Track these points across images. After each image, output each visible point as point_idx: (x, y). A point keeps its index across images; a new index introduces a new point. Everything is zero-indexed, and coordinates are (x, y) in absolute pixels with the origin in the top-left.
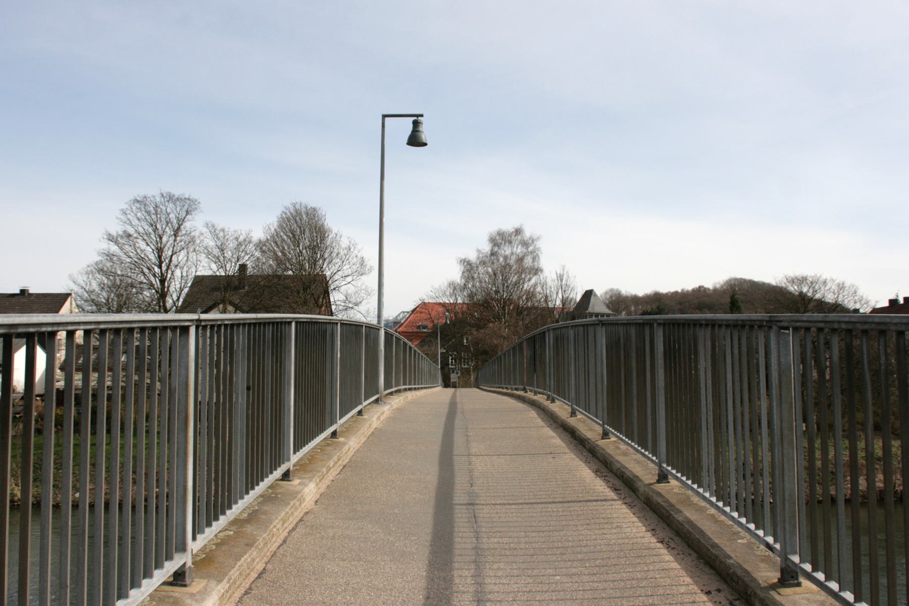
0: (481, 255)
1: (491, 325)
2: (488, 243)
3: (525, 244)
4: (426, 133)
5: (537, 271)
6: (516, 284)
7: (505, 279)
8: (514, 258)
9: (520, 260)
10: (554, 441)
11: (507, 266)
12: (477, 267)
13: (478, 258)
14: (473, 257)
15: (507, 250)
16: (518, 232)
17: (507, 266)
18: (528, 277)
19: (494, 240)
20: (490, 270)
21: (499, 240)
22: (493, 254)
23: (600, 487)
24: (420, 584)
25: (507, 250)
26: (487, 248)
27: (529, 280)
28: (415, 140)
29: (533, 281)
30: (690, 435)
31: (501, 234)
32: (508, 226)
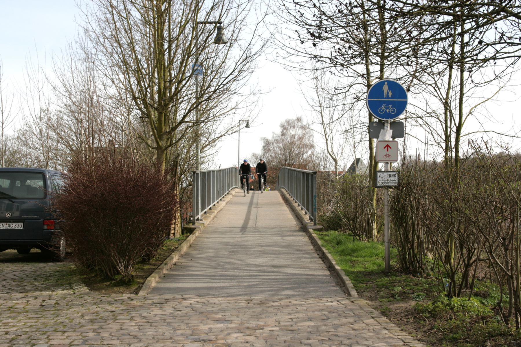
0: (275, 136)
1: (383, 278)
2: (280, 128)
3: (303, 128)
4: (251, 125)
5: (312, 146)
6: (298, 155)
7: (291, 152)
8: (296, 137)
9: (300, 139)
10: (289, 215)
11: (293, 143)
12: (273, 144)
13: (273, 137)
14: (270, 138)
15: (292, 132)
16: (299, 120)
17: (293, 143)
18: (306, 150)
19: (283, 126)
20: (281, 145)
21: (286, 126)
22: (283, 134)
23: (281, 201)
24: (246, 210)
25: (292, 132)
26: (278, 131)
27: (306, 152)
28: (247, 126)
29: (310, 152)
30: (407, 257)
31: (288, 122)
32: (292, 117)
